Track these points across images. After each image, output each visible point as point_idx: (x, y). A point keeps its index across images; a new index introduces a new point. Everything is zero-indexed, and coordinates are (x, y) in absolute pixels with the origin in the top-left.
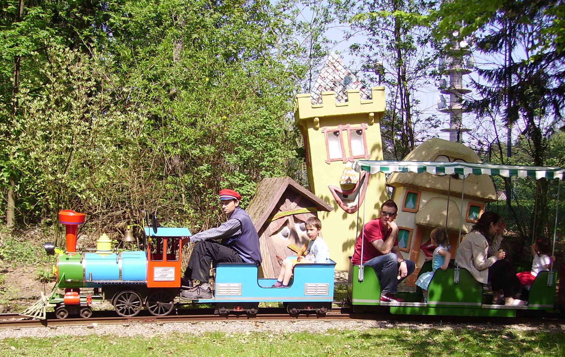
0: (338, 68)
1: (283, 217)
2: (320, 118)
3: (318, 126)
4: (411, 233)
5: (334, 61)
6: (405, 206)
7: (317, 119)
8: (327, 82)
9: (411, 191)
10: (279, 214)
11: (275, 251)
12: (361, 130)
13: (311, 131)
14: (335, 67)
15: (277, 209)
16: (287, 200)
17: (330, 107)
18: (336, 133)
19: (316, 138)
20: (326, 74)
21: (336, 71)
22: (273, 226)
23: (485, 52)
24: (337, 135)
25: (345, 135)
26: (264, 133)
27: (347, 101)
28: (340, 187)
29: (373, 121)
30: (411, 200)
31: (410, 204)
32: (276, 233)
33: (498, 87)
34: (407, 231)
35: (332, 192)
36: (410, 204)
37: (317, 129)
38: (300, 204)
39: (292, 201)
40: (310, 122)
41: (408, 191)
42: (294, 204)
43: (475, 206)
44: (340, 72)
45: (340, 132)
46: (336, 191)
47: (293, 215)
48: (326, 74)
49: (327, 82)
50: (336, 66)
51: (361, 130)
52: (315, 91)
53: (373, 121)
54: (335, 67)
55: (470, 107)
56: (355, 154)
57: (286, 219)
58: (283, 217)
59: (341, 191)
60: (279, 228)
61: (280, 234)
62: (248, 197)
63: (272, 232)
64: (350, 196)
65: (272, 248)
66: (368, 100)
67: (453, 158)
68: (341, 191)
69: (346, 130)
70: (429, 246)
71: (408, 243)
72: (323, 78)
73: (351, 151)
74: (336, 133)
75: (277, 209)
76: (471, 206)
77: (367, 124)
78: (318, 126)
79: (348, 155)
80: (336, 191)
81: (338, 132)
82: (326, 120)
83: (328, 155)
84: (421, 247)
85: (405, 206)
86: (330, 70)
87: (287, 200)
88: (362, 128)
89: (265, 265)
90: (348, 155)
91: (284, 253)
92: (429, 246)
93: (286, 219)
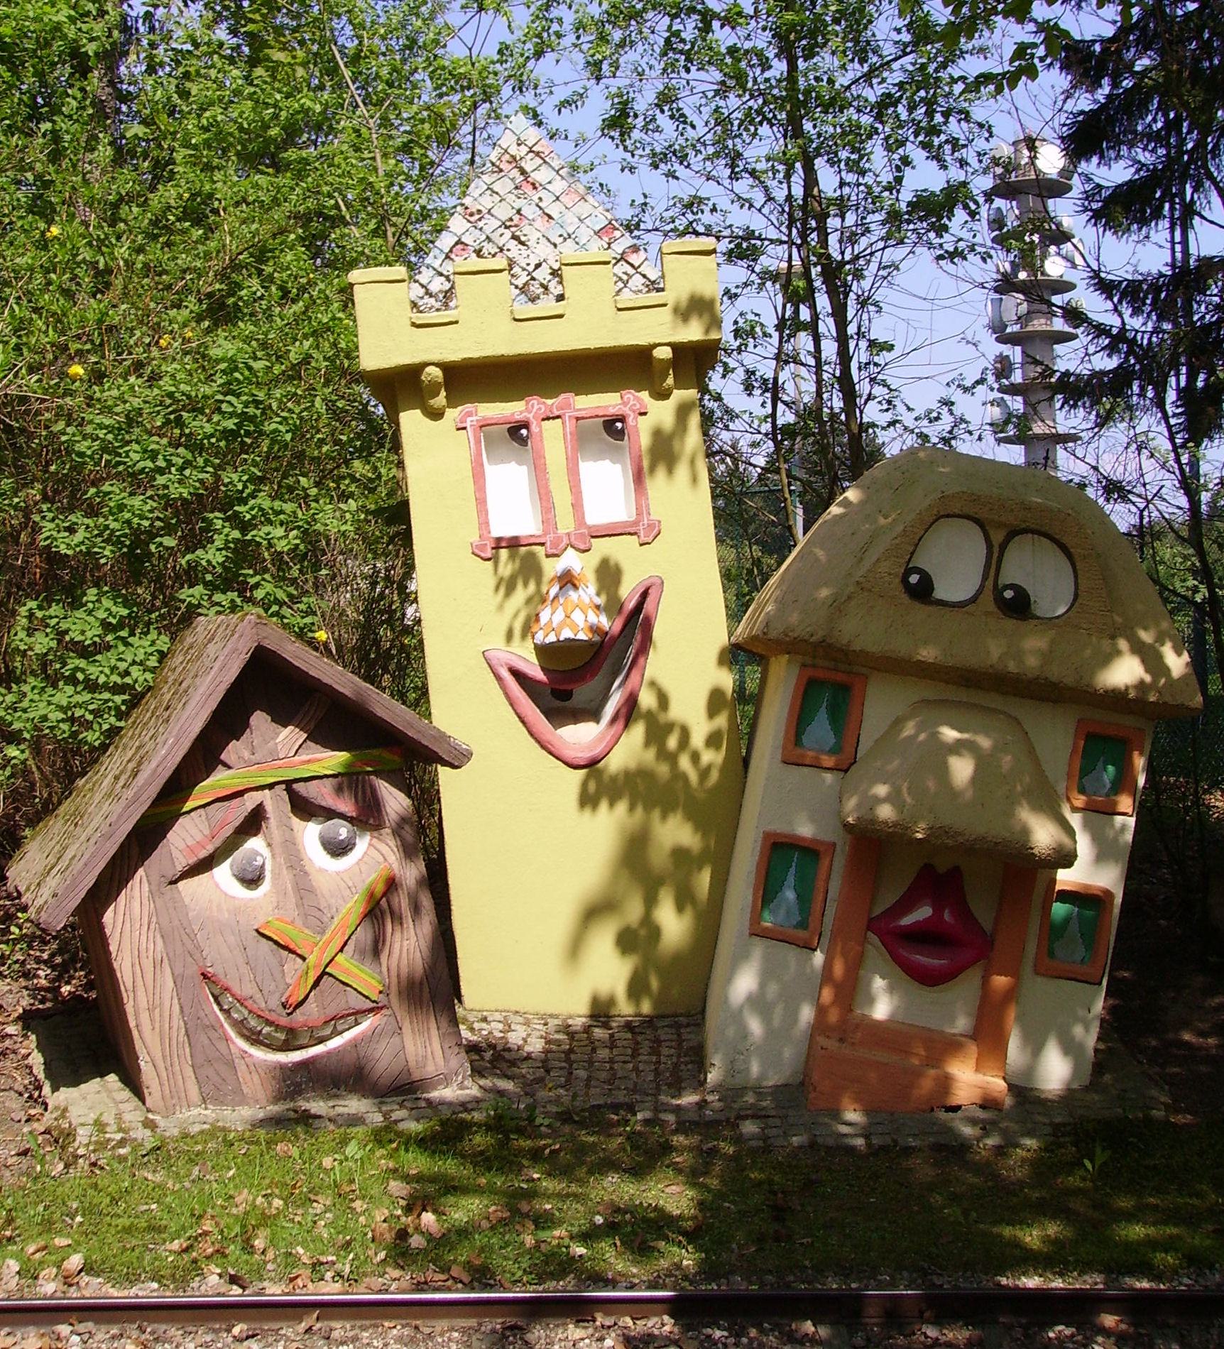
0: (535, 176)
1: (239, 794)
2: (447, 368)
3: (440, 400)
4: (825, 862)
5: (524, 150)
6: (798, 741)
7: (434, 373)
8: (488, 230)
9: (820, 674)
10: (219, 780)
11: (195, 951)
12: (622, 419)
13: (411, 421)
14: (523, 172)
15: (204, 754)
16: (259, 720)
17: (487, 326)
18: (517, 432)
19: (433, 449)
20: (487, 202)
21: (528, 189)
22: (188, 835)
23: (1115, 233)
24: (523, 441)
25: (552, 439)
26: (209, 429)
27: (561, 298)
28: (533, 658)
29: (670, 381)
30: (822, 717)
31: (820, 730)
32: (206, 865)
33: (1156, 331)
34: (809, 852)
35: (499, 678)
36: (820, 730)
37: (436, 415)
38: (322, 735)
39: (282, 719)
40: (402, 385)
41: (810, 672)
42: (289, 736)
43: (1105, 739)
44: (543, 194)
45: (534, 428)
46: (516, 673)
47: (289, 784)
48: (487, 202)
49: (488, 230)
50: (528, 168)
51: (622, 419)
52: (436, 264)
53: (670, 381)
54: (523, 172)
55: (1075, 390)
56: (595, 516)
57: (251, 801)
58: (239, 794)
59: (539, 675)
60: (218, 842)
61: (223, 874)
62: (118, 699)
63: (182, 863)
64: (583, 693)
65: (177, 934)
66: (654, 294)
67: (1000, 525)
68: (539, 675)
69: (555, 420)
70: (907, 921)
71: (817, 907)
72: (474, 217)
73: (577, 506)
74: (517, 432)
75: (204, 754)
76: (1091, 738)
77: (645, 395)
78: (440, 400)
79: (566, 524)
80: (516, 673)
81: (526, 425)
82: (472, 379)
83: (484, 524)
84: (872, 925)
85: (798, 741)
86: (503, 186)
87: (259, 720)
88: (626, 410)
89: (144, 1018)
90: (566, 524)
91: (241, 961)
92: (907, 921)
93: (251, 801)
